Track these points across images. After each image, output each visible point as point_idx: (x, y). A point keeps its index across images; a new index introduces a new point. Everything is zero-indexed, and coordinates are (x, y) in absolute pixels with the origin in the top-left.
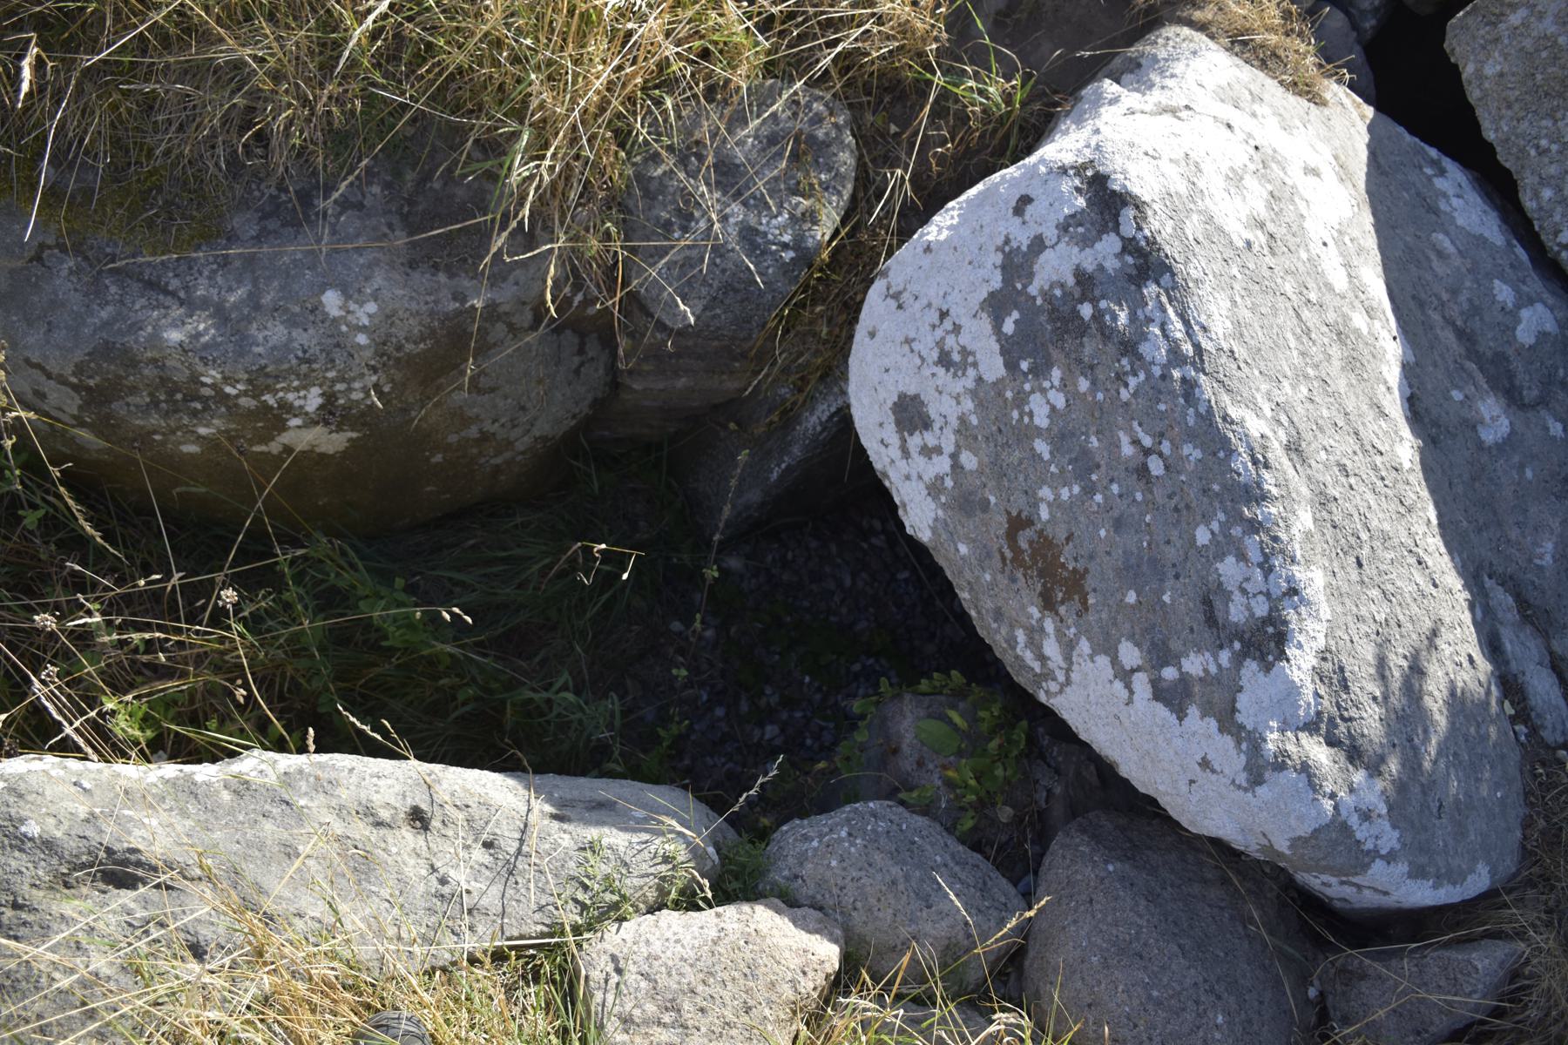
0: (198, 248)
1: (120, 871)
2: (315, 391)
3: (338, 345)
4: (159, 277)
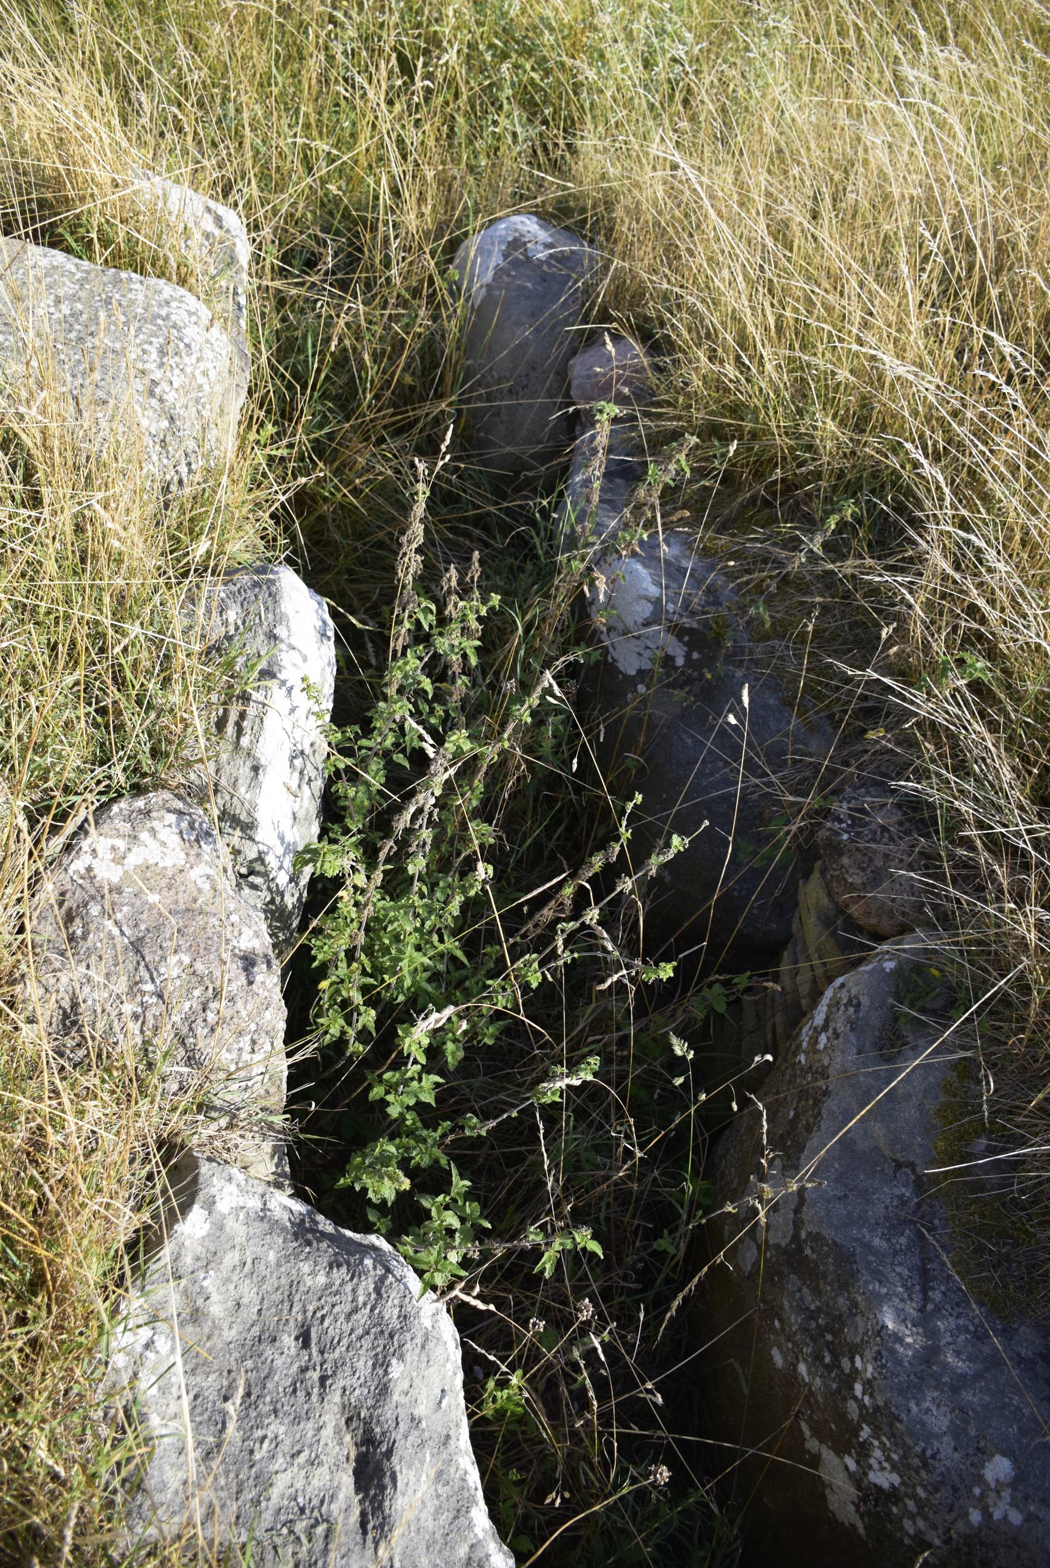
0: (981, 1304)
1: (372, 1472)
2: (895, 1479)
3: (955, 1490)
4: (935, 1278)
